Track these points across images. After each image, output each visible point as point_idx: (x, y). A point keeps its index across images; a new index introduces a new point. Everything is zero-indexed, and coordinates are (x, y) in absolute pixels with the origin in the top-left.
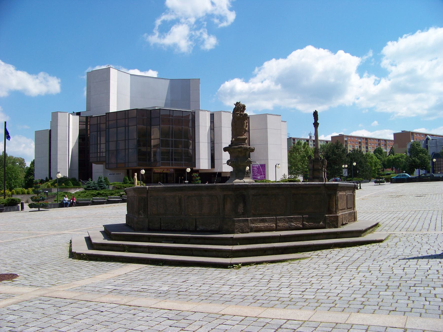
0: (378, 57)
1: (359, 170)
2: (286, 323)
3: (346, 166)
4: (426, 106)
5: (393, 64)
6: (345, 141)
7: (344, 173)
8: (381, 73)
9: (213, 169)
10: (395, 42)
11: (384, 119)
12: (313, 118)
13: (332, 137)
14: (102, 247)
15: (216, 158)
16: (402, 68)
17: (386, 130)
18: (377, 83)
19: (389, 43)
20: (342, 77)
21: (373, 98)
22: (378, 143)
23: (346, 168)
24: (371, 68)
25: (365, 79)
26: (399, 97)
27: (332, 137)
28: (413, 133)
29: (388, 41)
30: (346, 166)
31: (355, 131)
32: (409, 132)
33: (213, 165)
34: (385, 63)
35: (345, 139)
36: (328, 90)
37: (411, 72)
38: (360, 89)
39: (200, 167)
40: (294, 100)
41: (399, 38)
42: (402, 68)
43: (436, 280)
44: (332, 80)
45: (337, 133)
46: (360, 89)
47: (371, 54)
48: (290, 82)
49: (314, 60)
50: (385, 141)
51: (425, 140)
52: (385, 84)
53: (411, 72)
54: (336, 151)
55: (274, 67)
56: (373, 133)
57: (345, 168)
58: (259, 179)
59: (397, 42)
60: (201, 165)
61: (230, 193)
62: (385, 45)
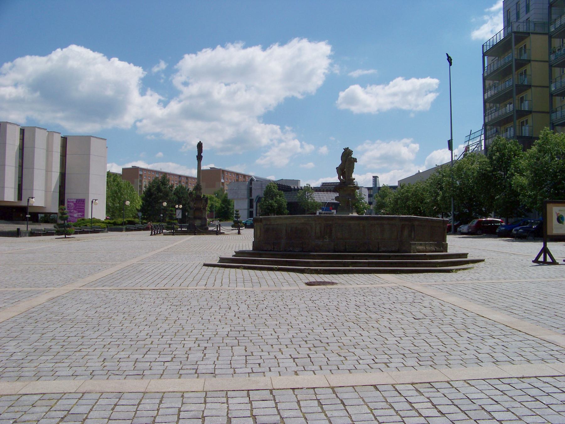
0: (171, 71)
1: (188, 211)
2: (56, 403)
3: (181, 206)
4: (221, 139)
5: (186, 84)
6: (140, 175)
7: (177, 214)
8: (169, 93)
9: (20, 201)
10: (193, 56)
11: (171, 148)
12: (196, 149)
13: (123, 169)
14: (320, 265)
15: (24, 187)
16: (194, 89)
17: (170, 164)
18: (164, 104)
19: (187, 56)
20: (121, 89)
21: (158, 122)
22: (178, 180)
23: (180, 209)
24: (159, 84)
25: (148, 98)
26: (190, 125)
27: (123, 169)
28: (223, 171)
29: (186, 53)
30: (181, 206)
31: (137, 161)
32: (220, 170)
33: (20, 197)
34: (178, 80)
35: (140, 173)
36: (104, 106)
37: (205, 95)
38: (143, 109)
39: (4, 198)
40: (60, 115)
41: (369, 85)
42: (194, 89)
43: (222, 344)
44: (110, 93)
45: (119, 164)
46: (143, 109)
47: (163, 65)
48: (50, 90)
49: (87, 65)
50: (187, 178)
51: (249, 180)
52: (175, 106)
53: (205, 95)
54: (162, 187)
55: (32, 65)
56: (152, 165)
57: (179, 208)
58: (76, 218)
59: (196, 55)
60: (6, 195)
61: (407, 223)
62: (182, 58)
